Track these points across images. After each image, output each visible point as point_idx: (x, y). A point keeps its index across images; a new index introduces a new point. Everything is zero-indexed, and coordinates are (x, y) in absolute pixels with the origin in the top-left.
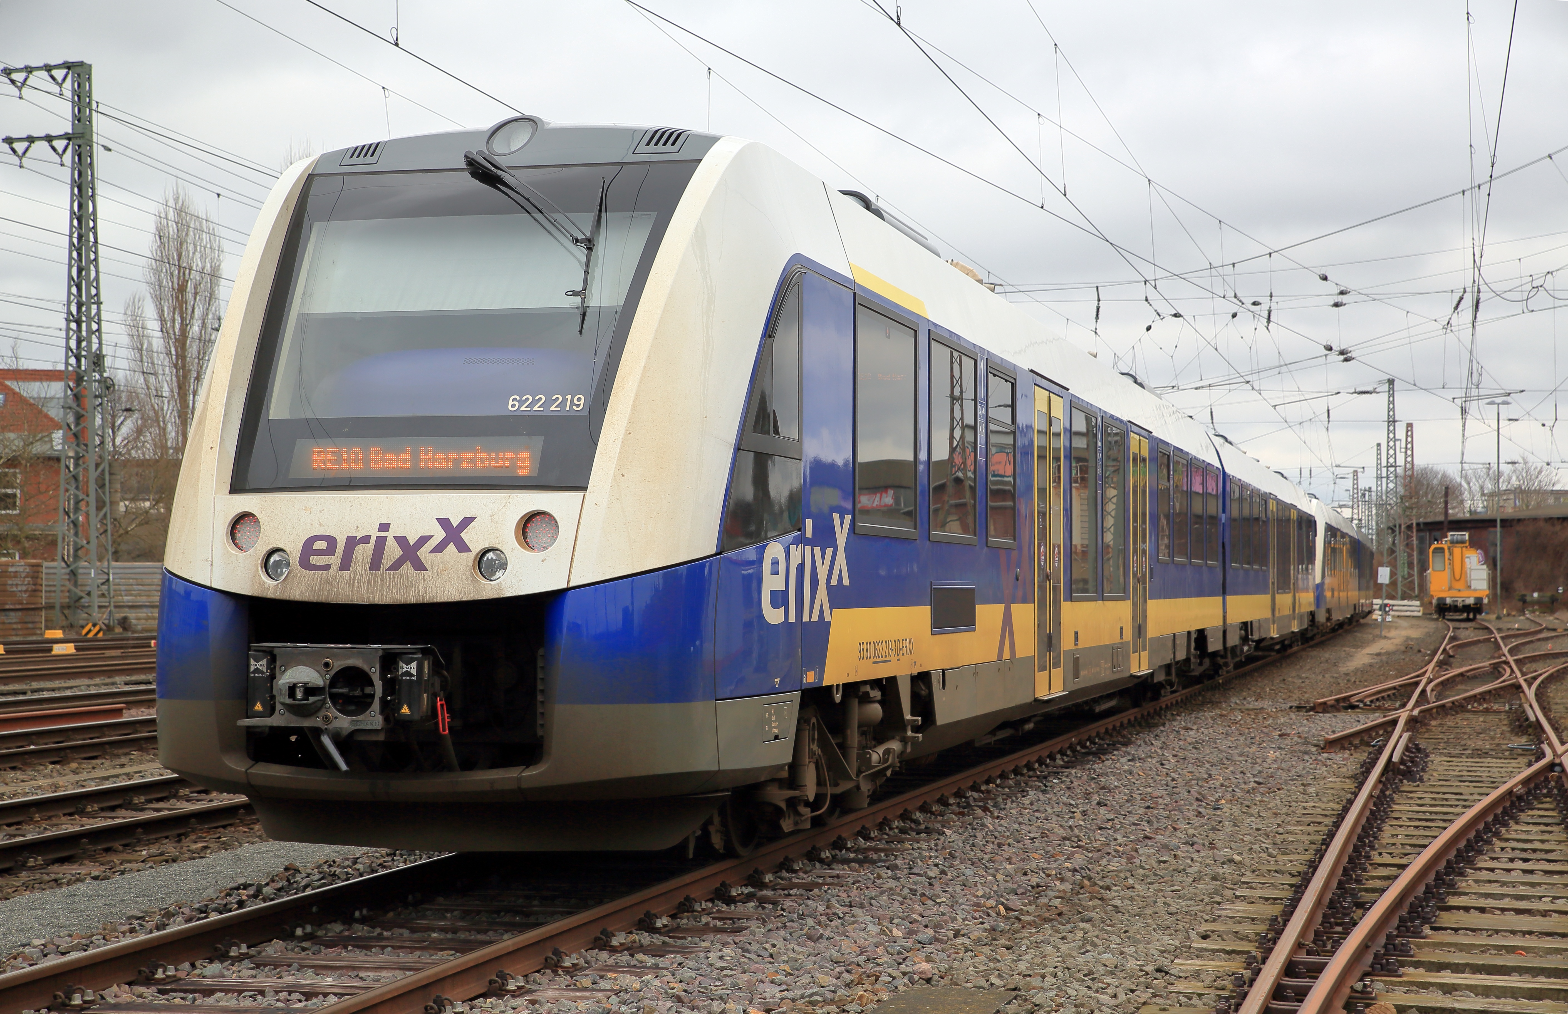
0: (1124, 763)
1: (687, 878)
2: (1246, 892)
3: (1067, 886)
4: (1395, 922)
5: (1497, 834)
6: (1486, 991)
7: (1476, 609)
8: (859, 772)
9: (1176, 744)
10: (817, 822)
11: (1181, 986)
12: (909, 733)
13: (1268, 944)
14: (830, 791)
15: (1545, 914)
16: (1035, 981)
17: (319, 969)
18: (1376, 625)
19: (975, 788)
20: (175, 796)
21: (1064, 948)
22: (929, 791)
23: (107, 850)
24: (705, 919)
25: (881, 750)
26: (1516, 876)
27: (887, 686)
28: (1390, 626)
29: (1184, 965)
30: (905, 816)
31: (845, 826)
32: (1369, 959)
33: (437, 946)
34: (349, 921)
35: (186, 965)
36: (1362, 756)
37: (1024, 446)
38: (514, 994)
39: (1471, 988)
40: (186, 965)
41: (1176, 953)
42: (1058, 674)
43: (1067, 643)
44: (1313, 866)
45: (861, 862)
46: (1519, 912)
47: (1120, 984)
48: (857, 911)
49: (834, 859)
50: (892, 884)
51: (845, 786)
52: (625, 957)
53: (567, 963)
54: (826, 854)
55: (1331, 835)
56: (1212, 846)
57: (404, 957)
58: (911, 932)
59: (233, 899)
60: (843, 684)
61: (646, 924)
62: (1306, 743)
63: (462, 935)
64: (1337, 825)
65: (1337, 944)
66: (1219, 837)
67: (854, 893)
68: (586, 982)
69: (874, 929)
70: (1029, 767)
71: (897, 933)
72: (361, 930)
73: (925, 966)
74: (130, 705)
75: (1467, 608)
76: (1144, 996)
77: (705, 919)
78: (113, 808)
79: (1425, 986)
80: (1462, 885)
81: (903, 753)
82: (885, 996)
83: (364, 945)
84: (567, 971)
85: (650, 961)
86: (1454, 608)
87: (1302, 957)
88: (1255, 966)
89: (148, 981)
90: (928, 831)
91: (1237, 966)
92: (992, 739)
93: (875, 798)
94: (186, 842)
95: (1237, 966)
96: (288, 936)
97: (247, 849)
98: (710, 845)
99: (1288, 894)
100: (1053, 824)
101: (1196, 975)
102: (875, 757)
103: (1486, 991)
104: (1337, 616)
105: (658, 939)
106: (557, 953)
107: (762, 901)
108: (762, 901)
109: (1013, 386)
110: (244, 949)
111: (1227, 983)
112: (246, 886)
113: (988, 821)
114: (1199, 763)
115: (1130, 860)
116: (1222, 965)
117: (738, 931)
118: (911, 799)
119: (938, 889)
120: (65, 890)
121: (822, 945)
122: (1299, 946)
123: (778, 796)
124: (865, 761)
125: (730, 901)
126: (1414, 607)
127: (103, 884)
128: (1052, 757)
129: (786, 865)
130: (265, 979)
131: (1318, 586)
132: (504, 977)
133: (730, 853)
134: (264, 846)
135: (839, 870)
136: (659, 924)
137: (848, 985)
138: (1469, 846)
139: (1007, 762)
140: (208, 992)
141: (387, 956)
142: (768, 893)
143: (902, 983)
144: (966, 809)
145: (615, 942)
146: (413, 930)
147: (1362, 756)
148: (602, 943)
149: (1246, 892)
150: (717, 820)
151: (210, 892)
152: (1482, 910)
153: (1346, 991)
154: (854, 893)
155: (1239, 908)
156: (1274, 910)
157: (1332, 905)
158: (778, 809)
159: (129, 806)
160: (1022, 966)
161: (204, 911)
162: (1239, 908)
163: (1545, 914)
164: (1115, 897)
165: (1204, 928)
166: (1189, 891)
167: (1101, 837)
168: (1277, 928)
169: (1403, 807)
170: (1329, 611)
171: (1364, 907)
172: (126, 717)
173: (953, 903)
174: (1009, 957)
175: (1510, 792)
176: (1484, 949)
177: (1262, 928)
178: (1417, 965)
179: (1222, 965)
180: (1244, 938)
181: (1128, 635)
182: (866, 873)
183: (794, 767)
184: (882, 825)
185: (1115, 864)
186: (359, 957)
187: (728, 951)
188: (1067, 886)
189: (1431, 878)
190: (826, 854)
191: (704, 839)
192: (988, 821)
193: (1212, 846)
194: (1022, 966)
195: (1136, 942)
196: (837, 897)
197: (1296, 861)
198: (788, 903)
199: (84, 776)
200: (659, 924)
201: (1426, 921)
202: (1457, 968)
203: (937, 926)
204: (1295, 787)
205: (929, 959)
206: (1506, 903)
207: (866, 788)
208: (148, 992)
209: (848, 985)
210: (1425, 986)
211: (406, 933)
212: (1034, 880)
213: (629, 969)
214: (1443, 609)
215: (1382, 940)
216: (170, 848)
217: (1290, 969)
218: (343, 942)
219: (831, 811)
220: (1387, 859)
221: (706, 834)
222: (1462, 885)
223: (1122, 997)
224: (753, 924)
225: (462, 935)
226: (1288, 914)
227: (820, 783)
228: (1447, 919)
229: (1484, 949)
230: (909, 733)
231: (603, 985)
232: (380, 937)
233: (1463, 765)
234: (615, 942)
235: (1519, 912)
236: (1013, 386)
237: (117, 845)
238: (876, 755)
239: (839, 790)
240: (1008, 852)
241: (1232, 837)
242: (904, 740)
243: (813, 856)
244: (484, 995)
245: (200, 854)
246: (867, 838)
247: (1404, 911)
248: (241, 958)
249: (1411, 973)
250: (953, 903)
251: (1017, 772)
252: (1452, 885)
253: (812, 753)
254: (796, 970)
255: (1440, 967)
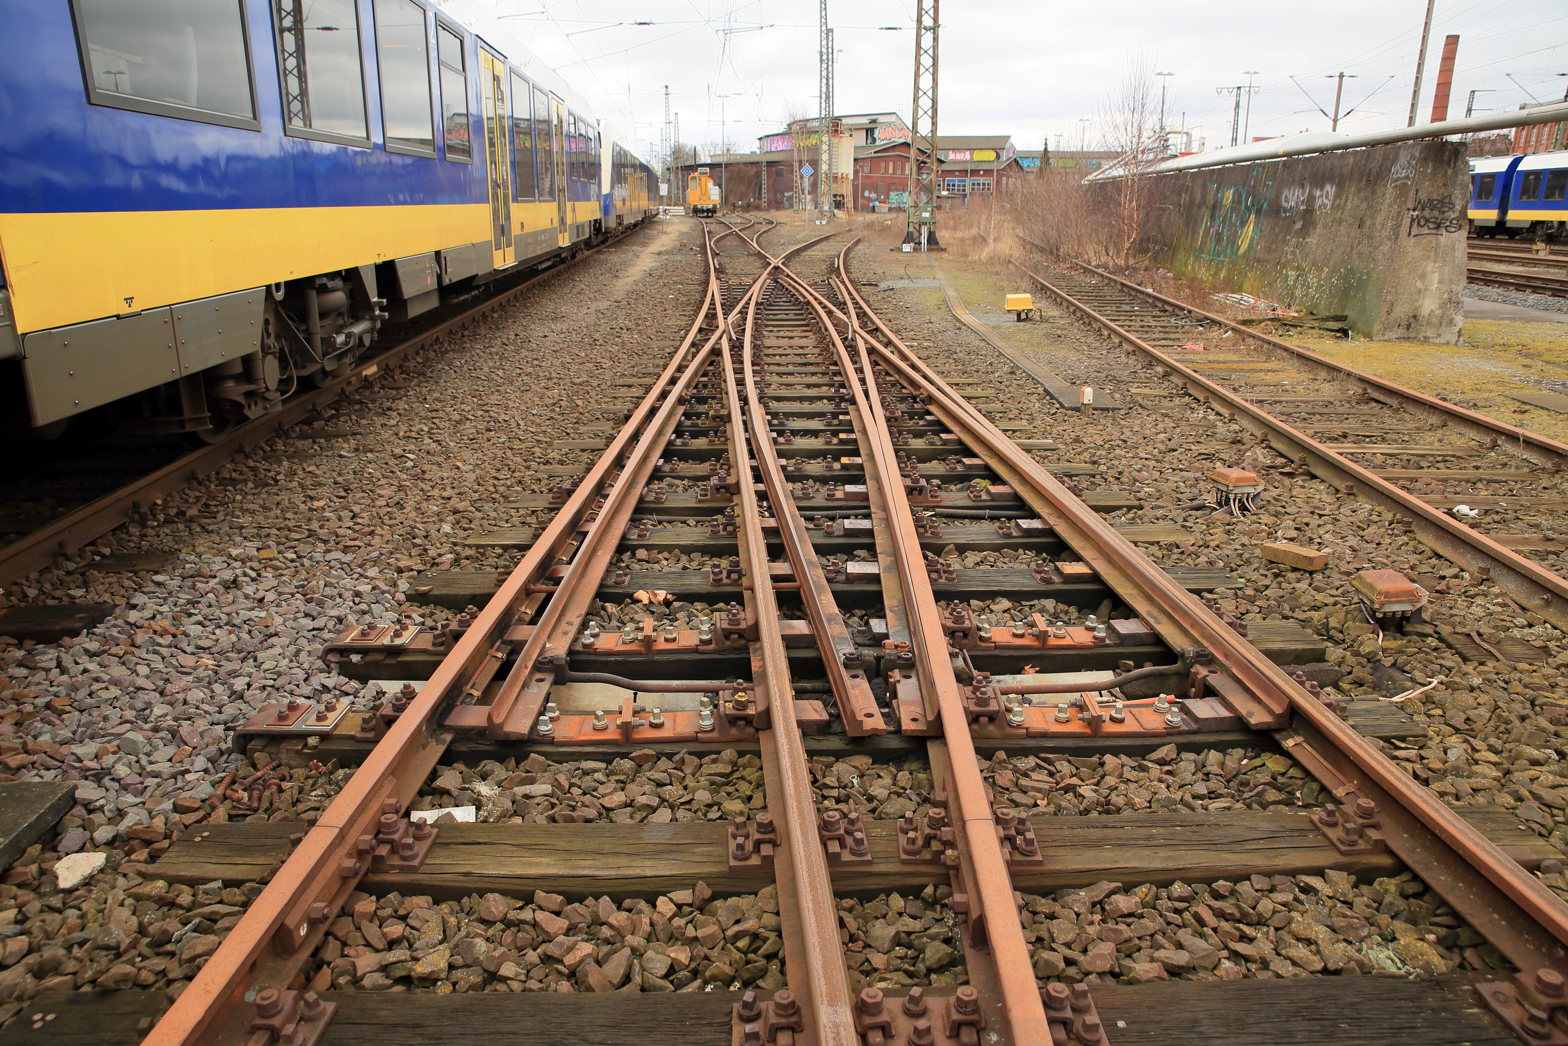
7: (713, 211)
8: (325, 354)
12: (377, 312)
18: (661, 222)
27: (351, 276)
28: (669, 223)
42: (567, 234)
43: (516, 230)
60: (286, 283)
75: (708, 211)
86: (702, 211)
104: (628, 220)
109: (462, 42)
123: (233, 390)
126: (680, 210)
131: (607, 196)
170: (619, 217)
181: (556, 223)
214: (696, 211)
230: (377, 312)
236: (462, 42)
239: (305, 373)
242: (373, 319)
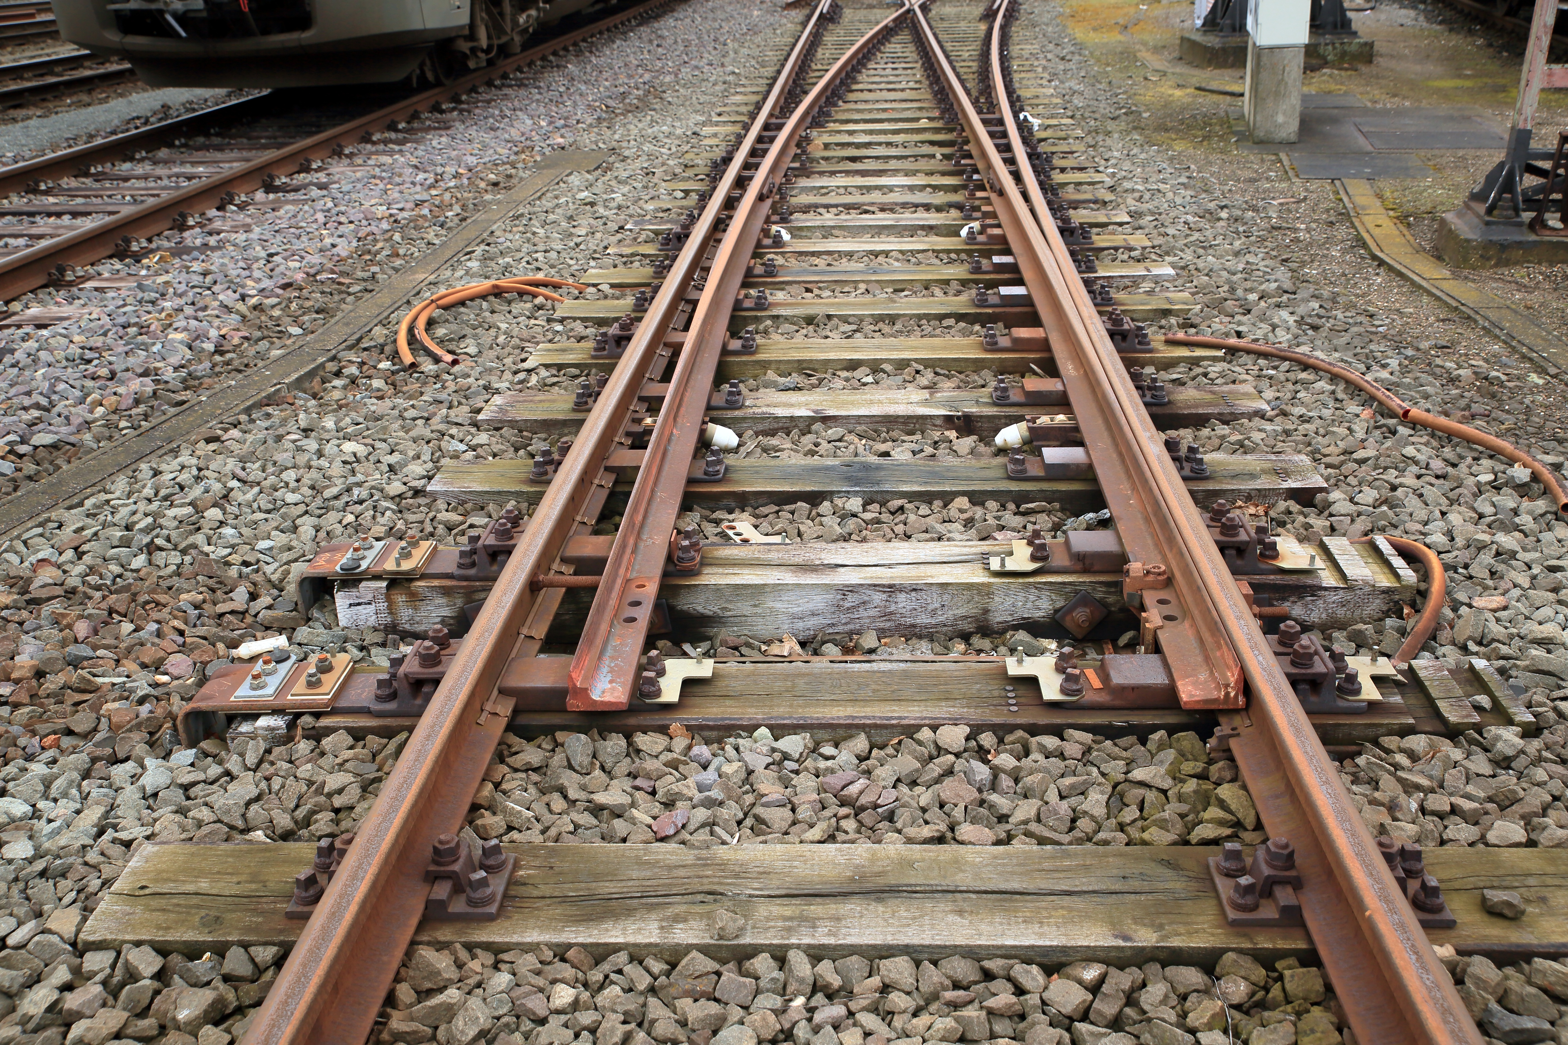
0: (671, 22)
1: (415, 99)
2: (742, 90)
3: (641, 92)
4: (824, 99)
5: (879, 50)
6: (871, 132)
9: (701, 10)
10: (490, 63)
11: (707, 142)
13: (753, 116)
14: (496, 42)
15: (903, 90)
16: (625, 144)
17: (194, 164)
19: (584, 40)
20: (82, 66)
21: (640, 125)
22: (556, 44)
23: (44, 100)
24: (428, 123)
25: (524, 16)
26: (888, 72)
29: (707, 130)
30: (544, 58)
31: (507, 65)
32: (809, 119)
33: (265, 147)
34: (207, 135)
35: (109, 165)
36: (806, 11)
37: (1330, 504)
38: (316, 171)
39: (864, 131)
40: (109, 165)
41: (704, 124)
44: (779, 72)
45: (519, 86)
46: (889, 90)
47: (673, 143)
48: (519, 113)
49: (503, 85)
50: (538, 97)
51: (504, 39)
52: (381, 147)
53: (347, 151)
54: (498, 82)
55: (789, 55)
56: (723, 65)
57: (245, 154)
58: (550, 123)
59: (131, 126)
61: (393, 127)
62: (775, 5)
63: (280, 140)
64: (792, 50)
65: (792, 112)
66: (726, 61)
67: (516, 103)
68: (360, 161)
69: (529, 122)
70: (616, 27)
71: (543, 123)
72: (217, 140)
73: (561, 140)
74: (40, 11)
76: (686, 148)
77: (428, 123)
78: (42, 75)
79: (839, 132)
80: (860, 78)
81: (538, 17)
82: (538, 158)
83: (220, 148)
84: (347, 156)
85: (397, 148)
87: (774, 121)
88: (747, 128)
89: (87, 174)
90: (558, 66)
91: (738, 129)
92: (591, 10)
93: (525, 47)
94: (94, 94)
95: (738, 129)
96: (171, 145)
97: (134, 97)
98: (426, 78)
99: (764, 89)
100: (632, 58)
101: (715, 135)
102: (521, 20)
103: (871, 132)
105: (400, 136)
106: (339, 146)
107: (461, 111)
108: (461, 111)
110: (144, 154)
111: (732, 138)
112: (138, 118)
113: (593, 59)
114: (714, 20)
115: (676, 75)
116: (729, 128)
117: (448, 128)
118: (546, 48)
119: (565, 98)
120: (20, 124)
121: (499, 133)
122: (771, 115)
123: (464, 46)
124: (515, 23)
125: (442, 112)
127: (45, 120)
128: (629, 21)
129: (474, 90)
130: (160, 171)
132: (309, 161)
133: (438, 84)
134: (146, 95)
135: (506, 91)
136: (400, 126)
137: (516, 153)
138: (864, 57)
139: (602, 24)
140: (126, 179)
141: (235, 154)
142: (465, 106)
143: (547, 151)
144: (579, 53)
145: (374, 138)
146: (249, 139)
147: (806, 11)
148: (366, 139)
149: (742, 90)
150: (428, 62)
151: (116, 122)
152: (870, 91)
153: (797, 137)
154: (516, 103)
155: (738, 98)
156: (759, 98)
157: (789, 92)
158: (465, 54)
159: (53, 74)
160: (617, 137)
161: (114, 133)
162: (738, 98)
163: (903, 90)
164: (668, 96)
165: (719, 110)
166: (710, 91)
167: (659, 64)
168: (759, 107)
169: (829, 38)
171: (806, 93)
172: (39, 19)
173: (575, 104)
174: (609, 133)
175: (886, 26)
176: (870, 111)
177: (751, 108)
178: (835, 121)
179: (729, 128)
180: (742, 114)
182: (522, 92)
183: (472, 26)
184: (530, 64)
185: (668, 79)
186: (219, 155)
187: (444, 139)
188: (641, 92)
189: (843, 75)
190: (498, 82)
191: (422, 76)
192: (593, 59)
193: (723, 65)
194: (617, 137)
195: (680, 119)
196: (506, 107)
197: (769, 71)
198: (477, 111)
199: (18, 56)
200: (400, 126)
201: (840, 98)
202: (856, 122)
203: (566, 118)
204: (769, 31)
205: (562, 136)
206: (883, 86)
207: (517, 39)
208: (88, 181)
209: (516, 153)
210: (839, 132)
211: (245, 141)
212: (622, 90)
213: (384, 153)
215: (816, 109)
216: (85, 98)
217: (766, 127)
218: (207, 148)
219: (498, 55)
220: (819, 67)
221: (423, 72)
222: (860, 78)
223: (674, 149)
224: (457, 124)
225: (280, 140)
226: (765, 99)
227: (489, 37)
228: (851, 96)
229: (870, 111)
231: (370, 162)
232: (229, 144)
233: (862, 14)
234: (374, 138)
235: (889, 90)
237: (49, 97)
238: (522, 19)
240: (605, 75)
241: (734, 60)
242: (538, 9)
243: (490, 84)
244: (299, 172)
245: (106, 100)
246: (522, 72)
247: (829, 93)
248: (142, 160)
249: (832, 126)
250: (575, 104)
251: (608, 30)
252: (854, 78)
253: (482, 19)
254: (485, 147)
255: (847, 121)
